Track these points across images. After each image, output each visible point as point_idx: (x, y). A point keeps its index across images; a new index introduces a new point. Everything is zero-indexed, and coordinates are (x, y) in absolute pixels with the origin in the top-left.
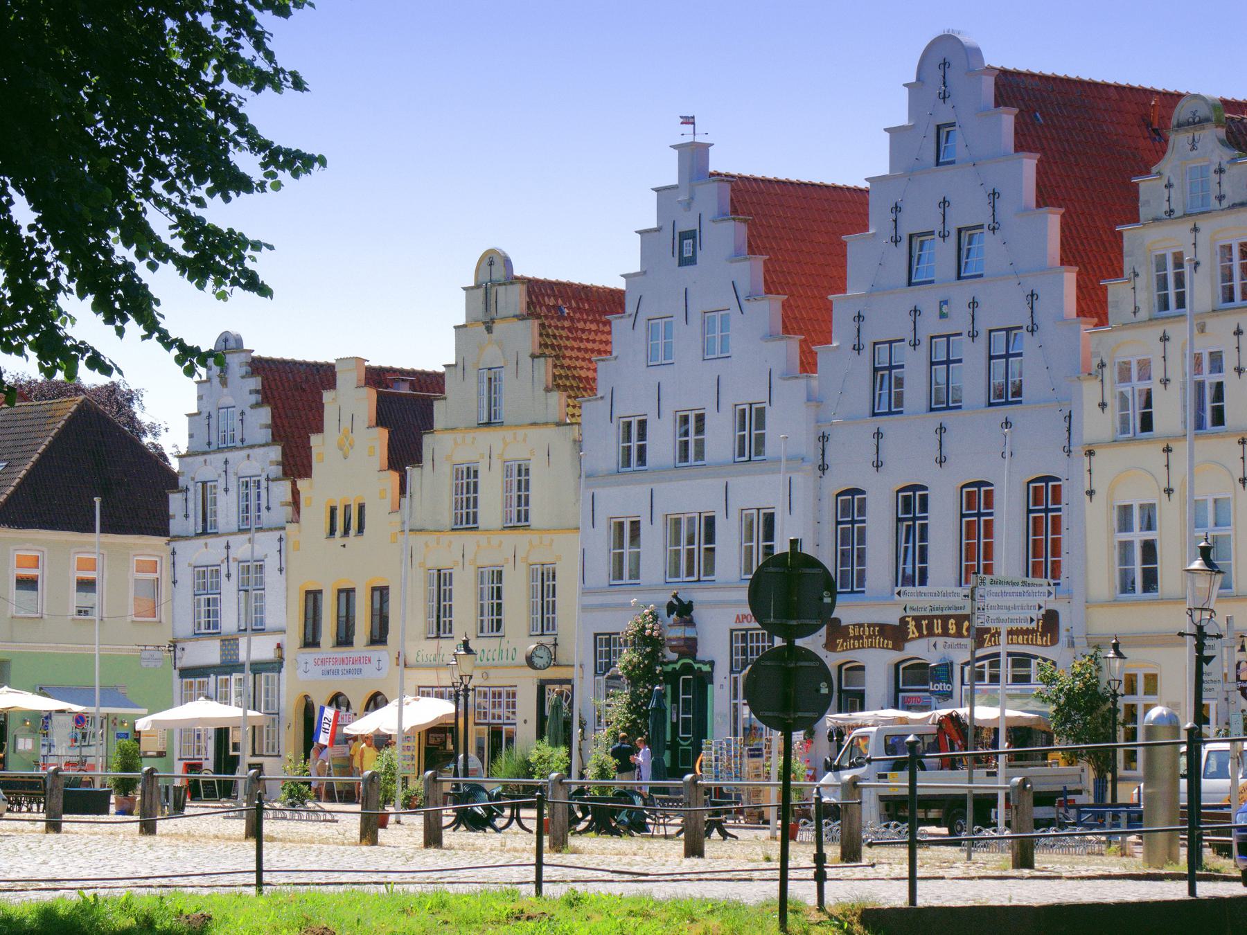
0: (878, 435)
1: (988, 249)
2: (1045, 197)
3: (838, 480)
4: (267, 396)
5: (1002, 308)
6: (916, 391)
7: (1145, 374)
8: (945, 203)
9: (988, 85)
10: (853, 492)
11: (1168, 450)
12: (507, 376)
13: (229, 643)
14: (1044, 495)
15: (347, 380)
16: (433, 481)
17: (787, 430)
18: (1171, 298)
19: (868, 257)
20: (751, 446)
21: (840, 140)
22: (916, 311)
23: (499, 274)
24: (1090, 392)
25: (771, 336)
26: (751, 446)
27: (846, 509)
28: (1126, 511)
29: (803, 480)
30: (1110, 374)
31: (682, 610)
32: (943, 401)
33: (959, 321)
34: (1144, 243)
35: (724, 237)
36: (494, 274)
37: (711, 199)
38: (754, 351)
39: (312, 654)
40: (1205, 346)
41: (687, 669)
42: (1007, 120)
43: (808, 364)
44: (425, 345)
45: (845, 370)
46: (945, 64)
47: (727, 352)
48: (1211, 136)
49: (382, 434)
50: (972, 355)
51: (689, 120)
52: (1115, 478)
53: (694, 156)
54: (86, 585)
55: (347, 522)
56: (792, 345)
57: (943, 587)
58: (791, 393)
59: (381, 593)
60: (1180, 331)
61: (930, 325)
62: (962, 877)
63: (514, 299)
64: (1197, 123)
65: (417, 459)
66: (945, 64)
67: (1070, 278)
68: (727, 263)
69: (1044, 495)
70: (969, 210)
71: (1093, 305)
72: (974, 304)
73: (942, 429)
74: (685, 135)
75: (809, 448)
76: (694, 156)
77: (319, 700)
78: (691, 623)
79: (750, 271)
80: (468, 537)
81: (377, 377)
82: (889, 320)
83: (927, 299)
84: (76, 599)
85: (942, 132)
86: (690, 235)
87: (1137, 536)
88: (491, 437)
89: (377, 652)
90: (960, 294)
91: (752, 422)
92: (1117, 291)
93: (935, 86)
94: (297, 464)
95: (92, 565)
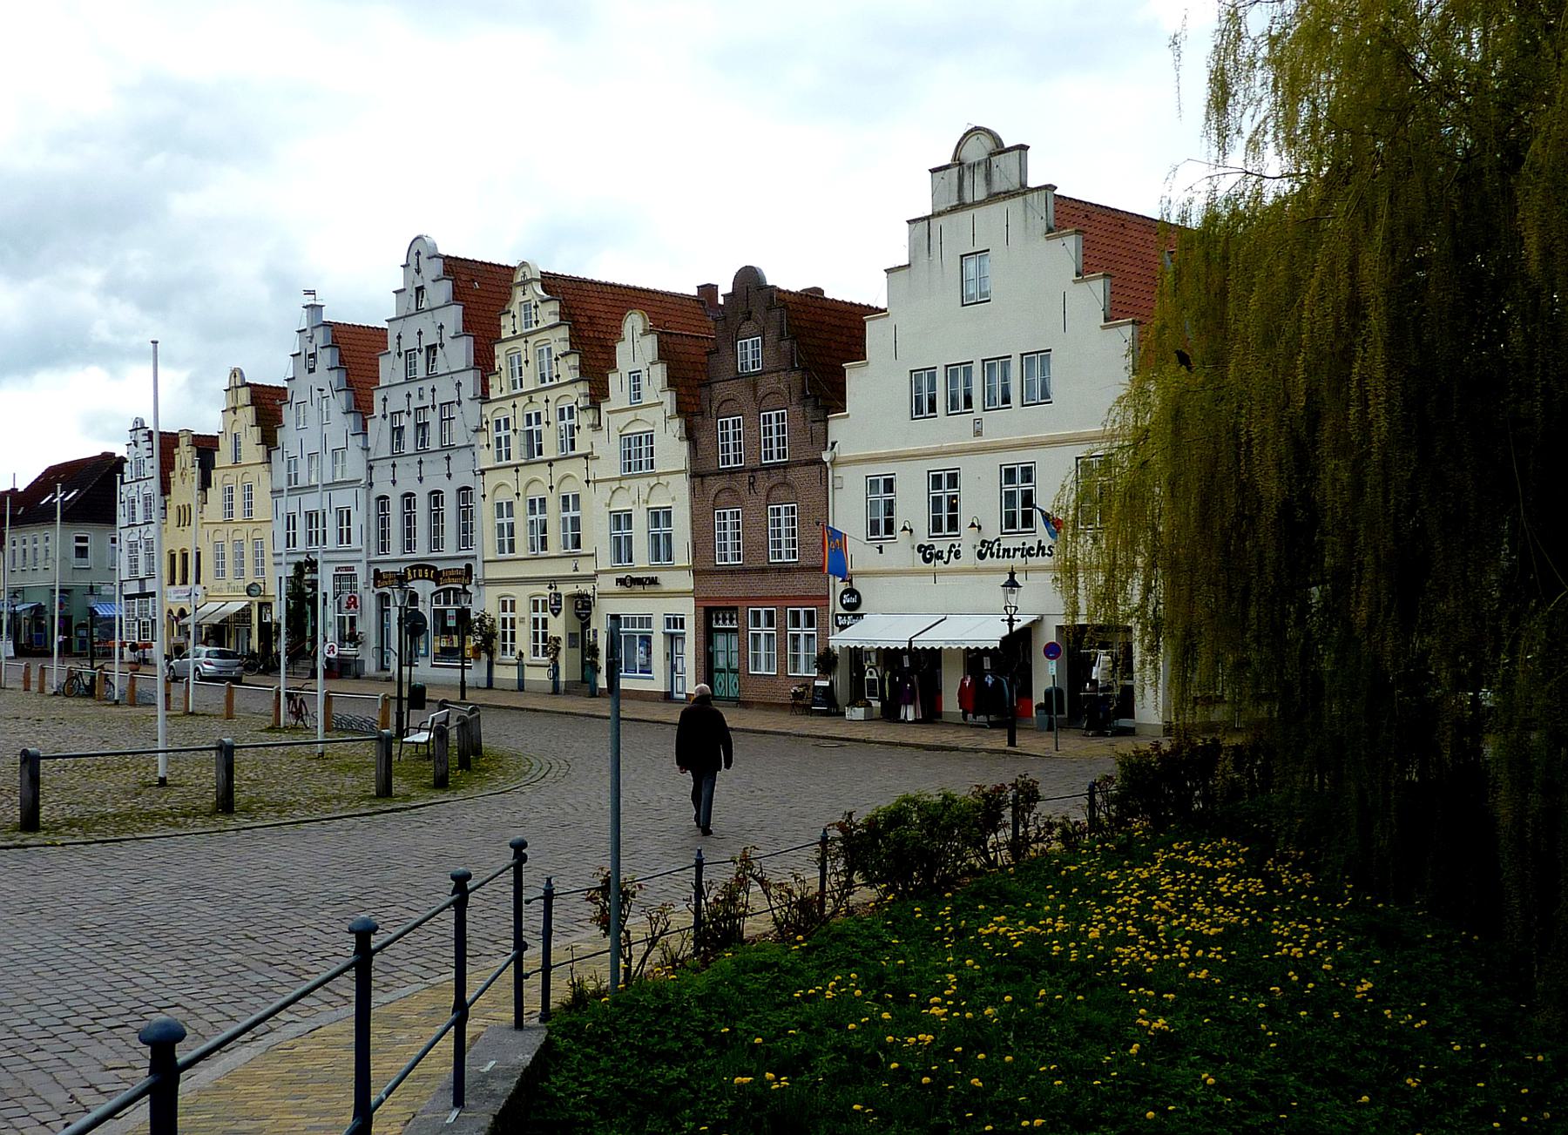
0: (394, 465)
4: (568, 315)
5: (446, 393)
8: (420, 333)
11: (483, 472)
13: (142, 586)
15: (183, 441)
22: (409, 395)
39: (172, 588)
40: (532, 410)
44: (209, 421)
46: (418, 253)
47: (320, 421)
51: (309, 293)
52: (501, 486)
57: (422, 551)
61: (415, 403)
62: (5, 618)
72: (433, 390)
74: (309, 300)
75: (362, 475)
82: (397, 401)
83: (413, 389)
87: (1019, 487)
94: (598, 394)
95: (85, 540)
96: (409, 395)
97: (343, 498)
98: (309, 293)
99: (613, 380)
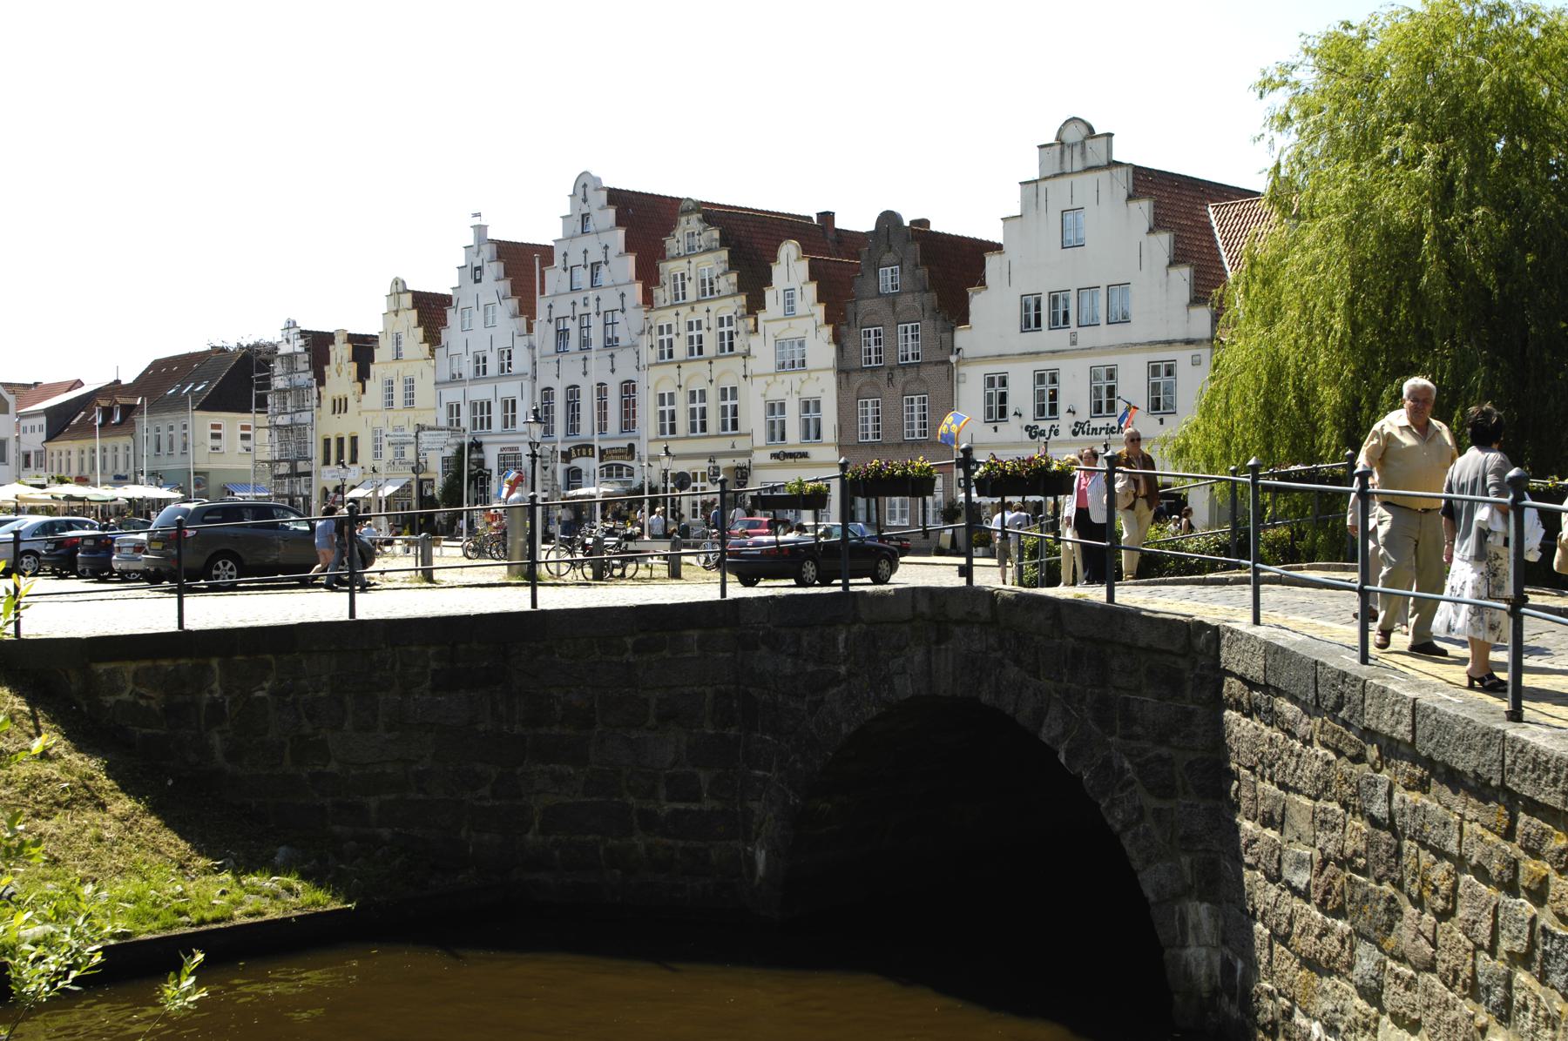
1: (604, 275)
2: (629, 247)
3: (543, 382)
5: (610, 300)
6: (574, 343)
7: (699, 327)
8: (585, 252)
9: (604, 194)
10: (575, 386)
12: (404, 339)
14: (628, 388)
15: (339, 340)
16: (374, 385)
17: (521, 362)
18: (679, 299)
19: (555, 278)
20: (505, 369)
21: (539, 222)
22: (574, 303)
23: (400, 289)
24: (645, 341)
25: (514, 316)
26: (505, 369)
27: (599, 391)
28: (693, 393)
29: (527, 385)
30: (655, 331)
31: (477, 446)
32: (585, 344)
33: (592, 309)
34: (669, 268)
35: (493, 270)
36: (399, 288)
37: (488, 252)
38: (505, 324)
39: (326, 469)
41: (480, 473)
42: (612, 212)
43: (530, 329)
44: (369, 323)
45: (544, 333)
46: (585, 186)
48: (695, 217)
49: (355, 365)
50: (596, 324)
51: (476, 215)
53: (480, 230)
54: (216, 436)
55: (340, 406)
56: (523, 320)
58: (521, 343)
59: (354, 440)
60: (684, 311)
61: (580, 309)
63: (407, 300)
64: (687, 212)
65: (368, 377)
66: (585, 186)
67: (639, 287)
68: (494, 283)
69: (628, 388)
70: (596, 255)
71: (648, 299)
73: (612, 356)
74: (477, 221)
75: (529, 369)
76: (480, 230)
77: (330, 489)
78: (481, 452)
79: (505, 286)
80: (389, 413)
81: (352, 338)
82: (562, 308)
83: (579, 298)
84: (211, 443)
85: (585, 218)
86: (478, 268)
88: (399, 365)
89: (353, 467)
90: (592, 295)
91: (507, 355)
92: (658, 292)
93: (581, 196)
94: (755, 304)
95: (219, 427)
96: (574, 303)
97: (509, 389)
98: (476, 215)
99: (769, 295)
